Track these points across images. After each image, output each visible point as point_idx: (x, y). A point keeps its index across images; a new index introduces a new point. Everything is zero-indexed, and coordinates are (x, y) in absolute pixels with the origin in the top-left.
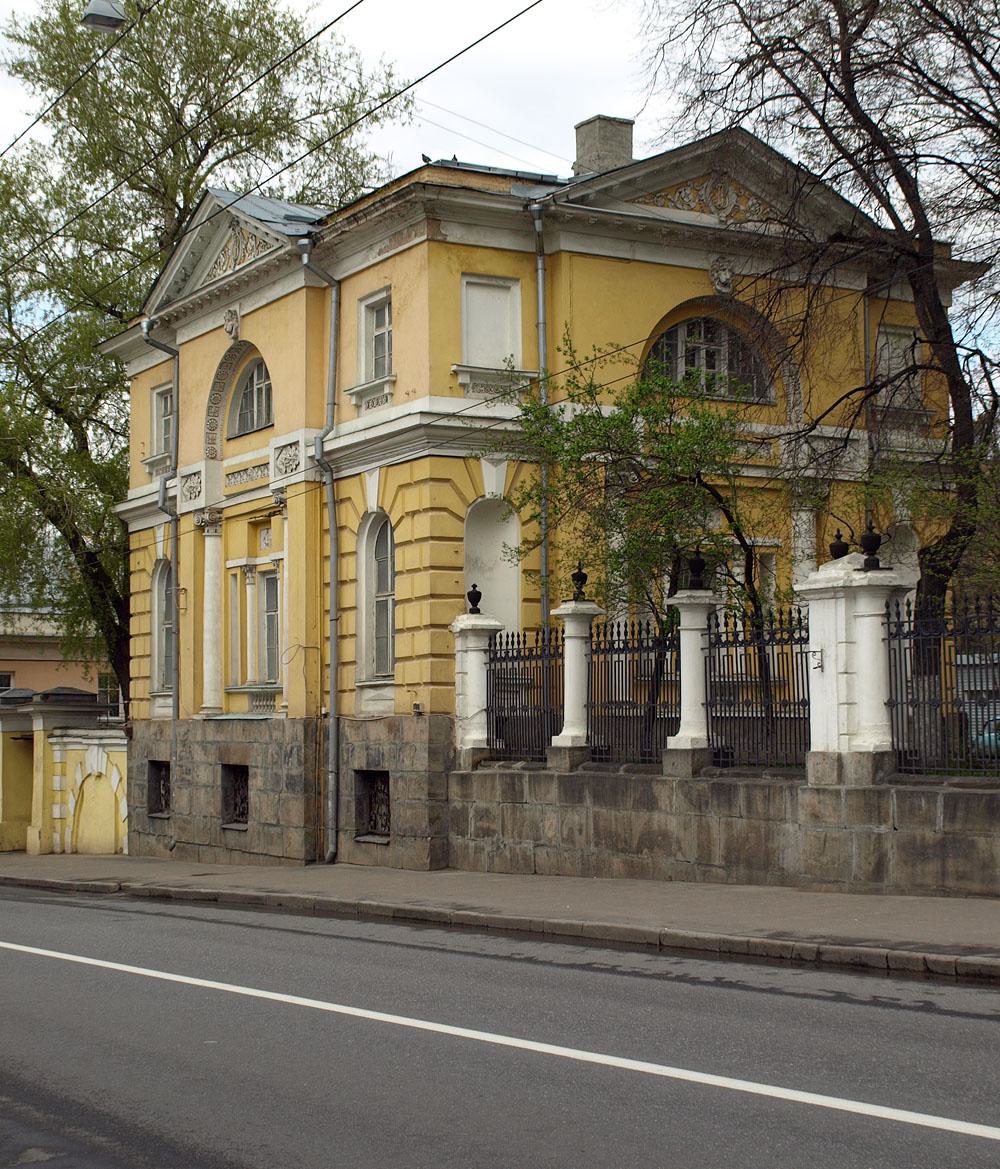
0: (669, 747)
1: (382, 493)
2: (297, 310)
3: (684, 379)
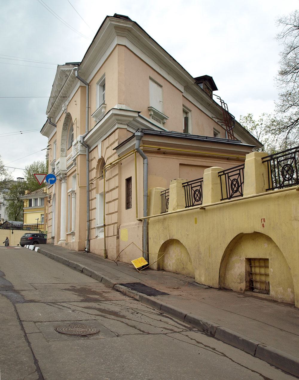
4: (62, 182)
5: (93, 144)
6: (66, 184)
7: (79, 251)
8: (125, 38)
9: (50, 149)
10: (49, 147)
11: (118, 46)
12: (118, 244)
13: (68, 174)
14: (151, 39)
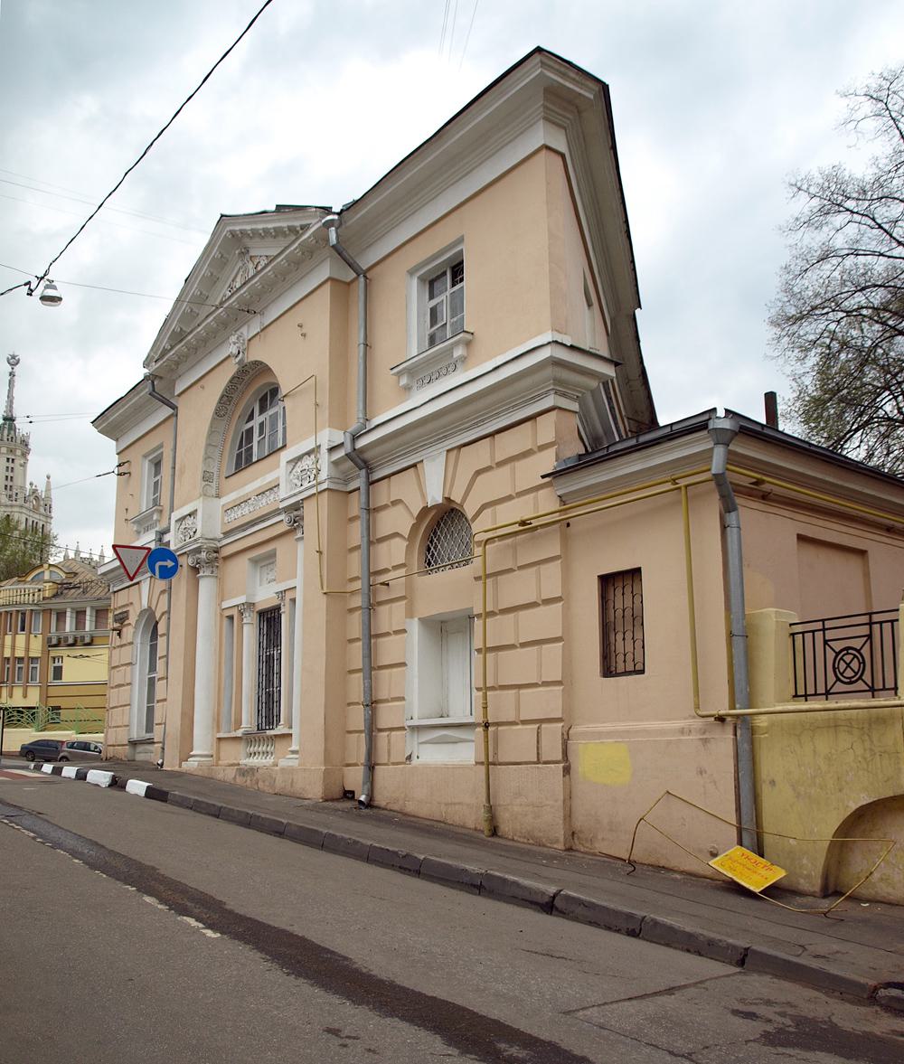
0: (661, 424)
1: (449, 481)
2: (319, 315)
3: (233, 233)
4: (201, 574)
5: (382, 464)
6: (213, 580)
7: (326, 800)
8: (564, 131)
9: (125, 474)
10: (123, 469)
11: (544, 151)
12: (568, 791)
13: (226, 552)
14: (612, 152)
